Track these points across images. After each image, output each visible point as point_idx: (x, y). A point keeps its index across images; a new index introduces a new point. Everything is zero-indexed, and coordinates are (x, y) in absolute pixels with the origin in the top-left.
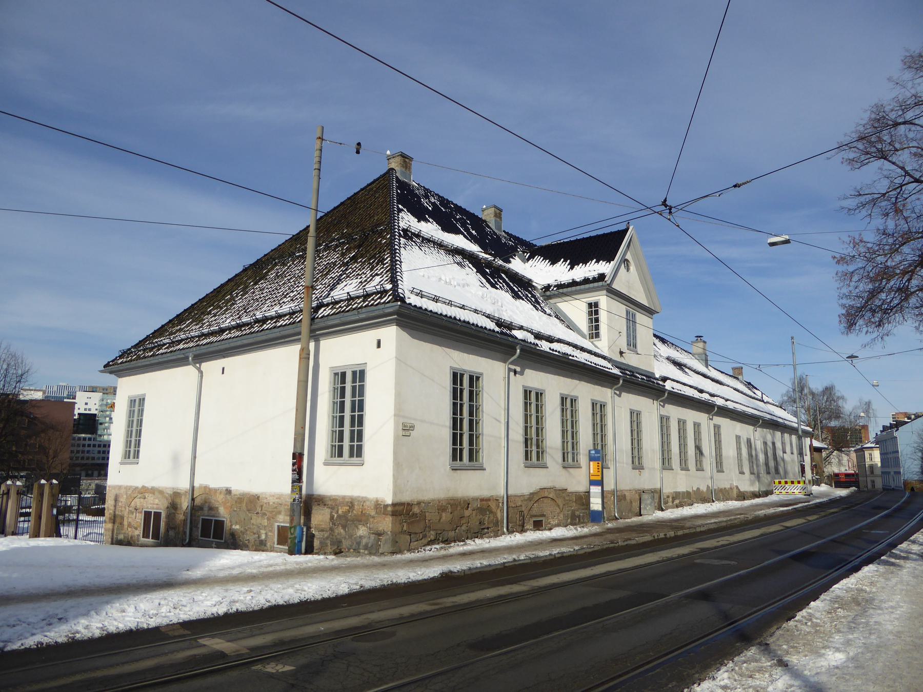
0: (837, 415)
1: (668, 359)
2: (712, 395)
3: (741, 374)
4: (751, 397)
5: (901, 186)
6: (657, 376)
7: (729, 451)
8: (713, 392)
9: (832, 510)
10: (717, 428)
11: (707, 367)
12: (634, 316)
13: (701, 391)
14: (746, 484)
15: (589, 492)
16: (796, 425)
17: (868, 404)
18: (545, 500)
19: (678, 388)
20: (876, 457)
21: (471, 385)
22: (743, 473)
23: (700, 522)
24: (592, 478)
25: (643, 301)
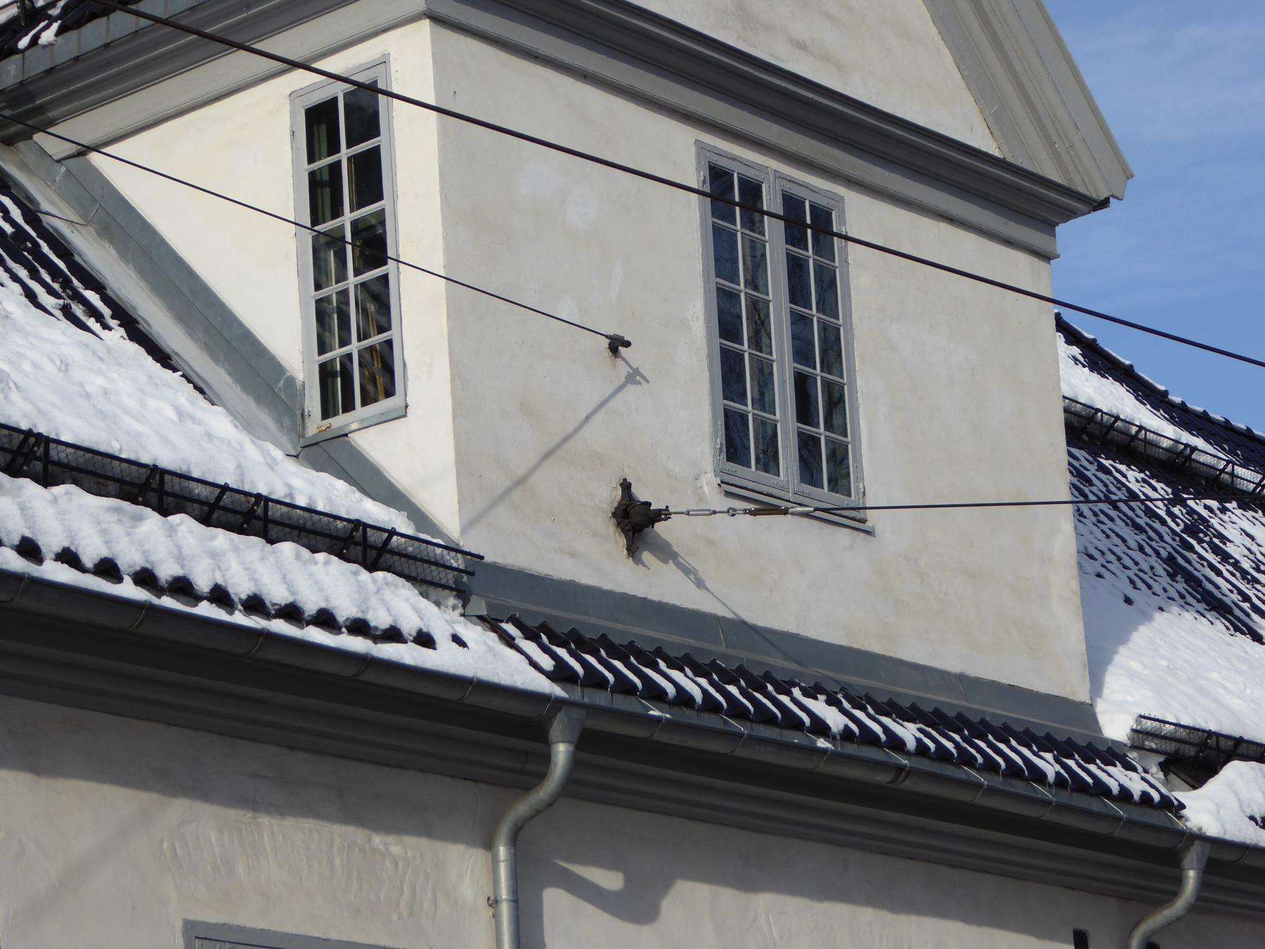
6: (1116, 726)
12: (812, 226)
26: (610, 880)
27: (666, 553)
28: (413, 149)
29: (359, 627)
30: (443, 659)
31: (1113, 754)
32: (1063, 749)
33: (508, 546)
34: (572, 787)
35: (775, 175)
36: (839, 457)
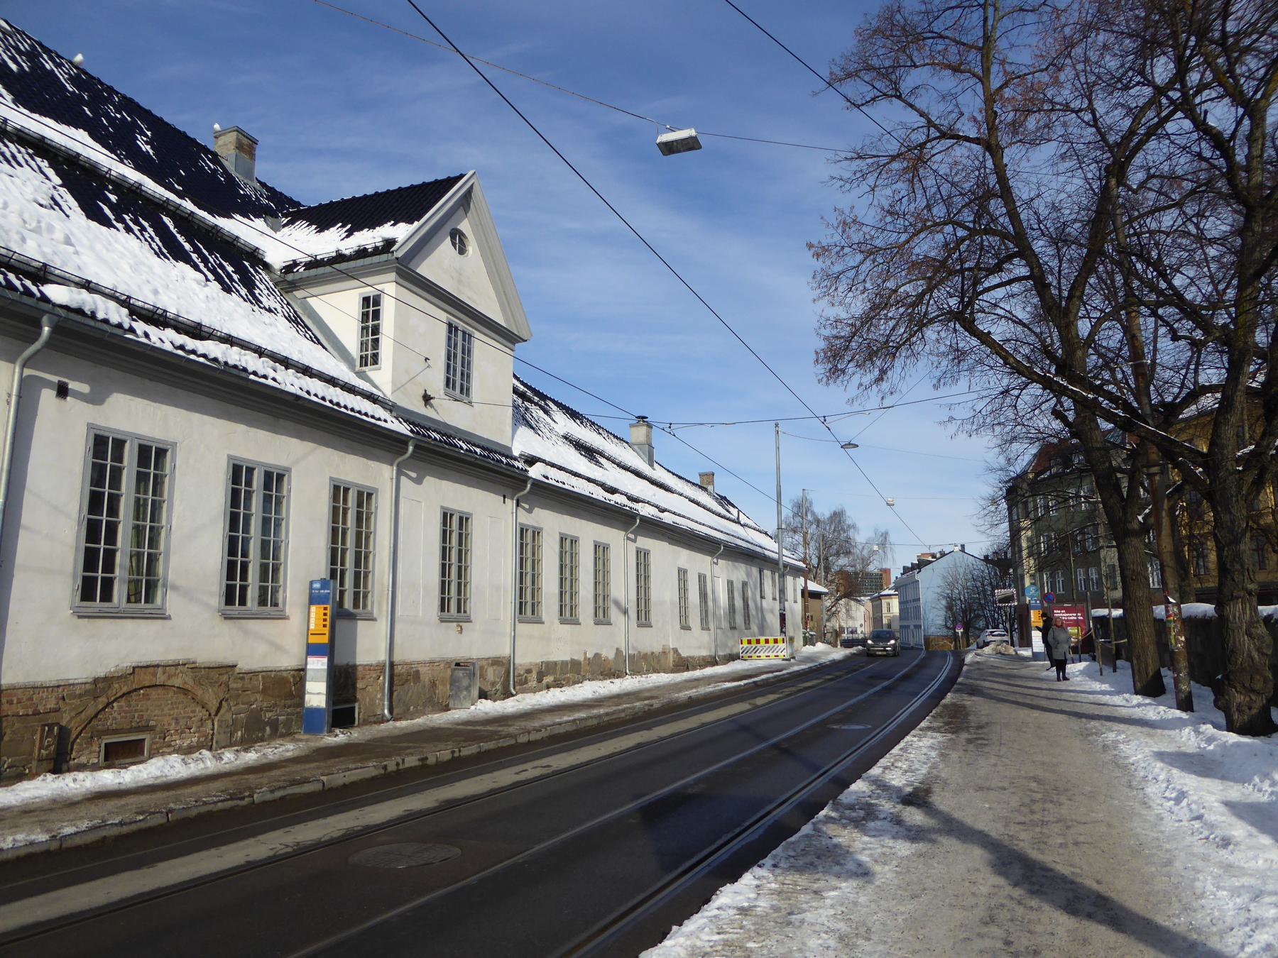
0: (845, 548)
1: (565, 437)
2: (630, 498)
3: (712, 482)
4: (719, 515)
5: (922, 146)
6: (516, 453)
7: (663, 591)
8: (664, 505)
9: (809, 684)
10: (643, 557)
11: (651, 465)
12: (467, 337)
13: (613, 491)
14: (696, 643)
15: (304, 670)
16: (776, 556)
17: (885, 535)
18: (154, 693)
19: (555, 477)
20: (893, 607)
21: (360, 505)
22: (689, 628)
23: (548, 720)
24: (313, 640)
25: (494, 312)
26: (414, 475)
27: (432, 406)
28: (388, 309)
29: (373, 417)
30: (389, 425)
31: (515, 459)
32: (507, 457)
33: (402, 402)
34: (49, 344)
35: (461, 325)
36: (468, 389)
